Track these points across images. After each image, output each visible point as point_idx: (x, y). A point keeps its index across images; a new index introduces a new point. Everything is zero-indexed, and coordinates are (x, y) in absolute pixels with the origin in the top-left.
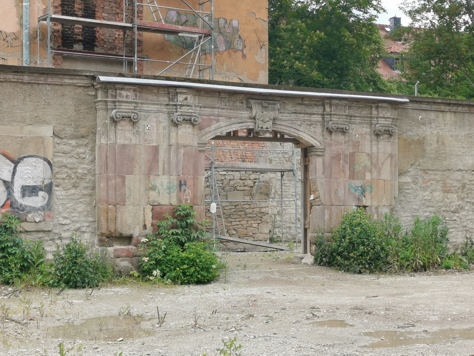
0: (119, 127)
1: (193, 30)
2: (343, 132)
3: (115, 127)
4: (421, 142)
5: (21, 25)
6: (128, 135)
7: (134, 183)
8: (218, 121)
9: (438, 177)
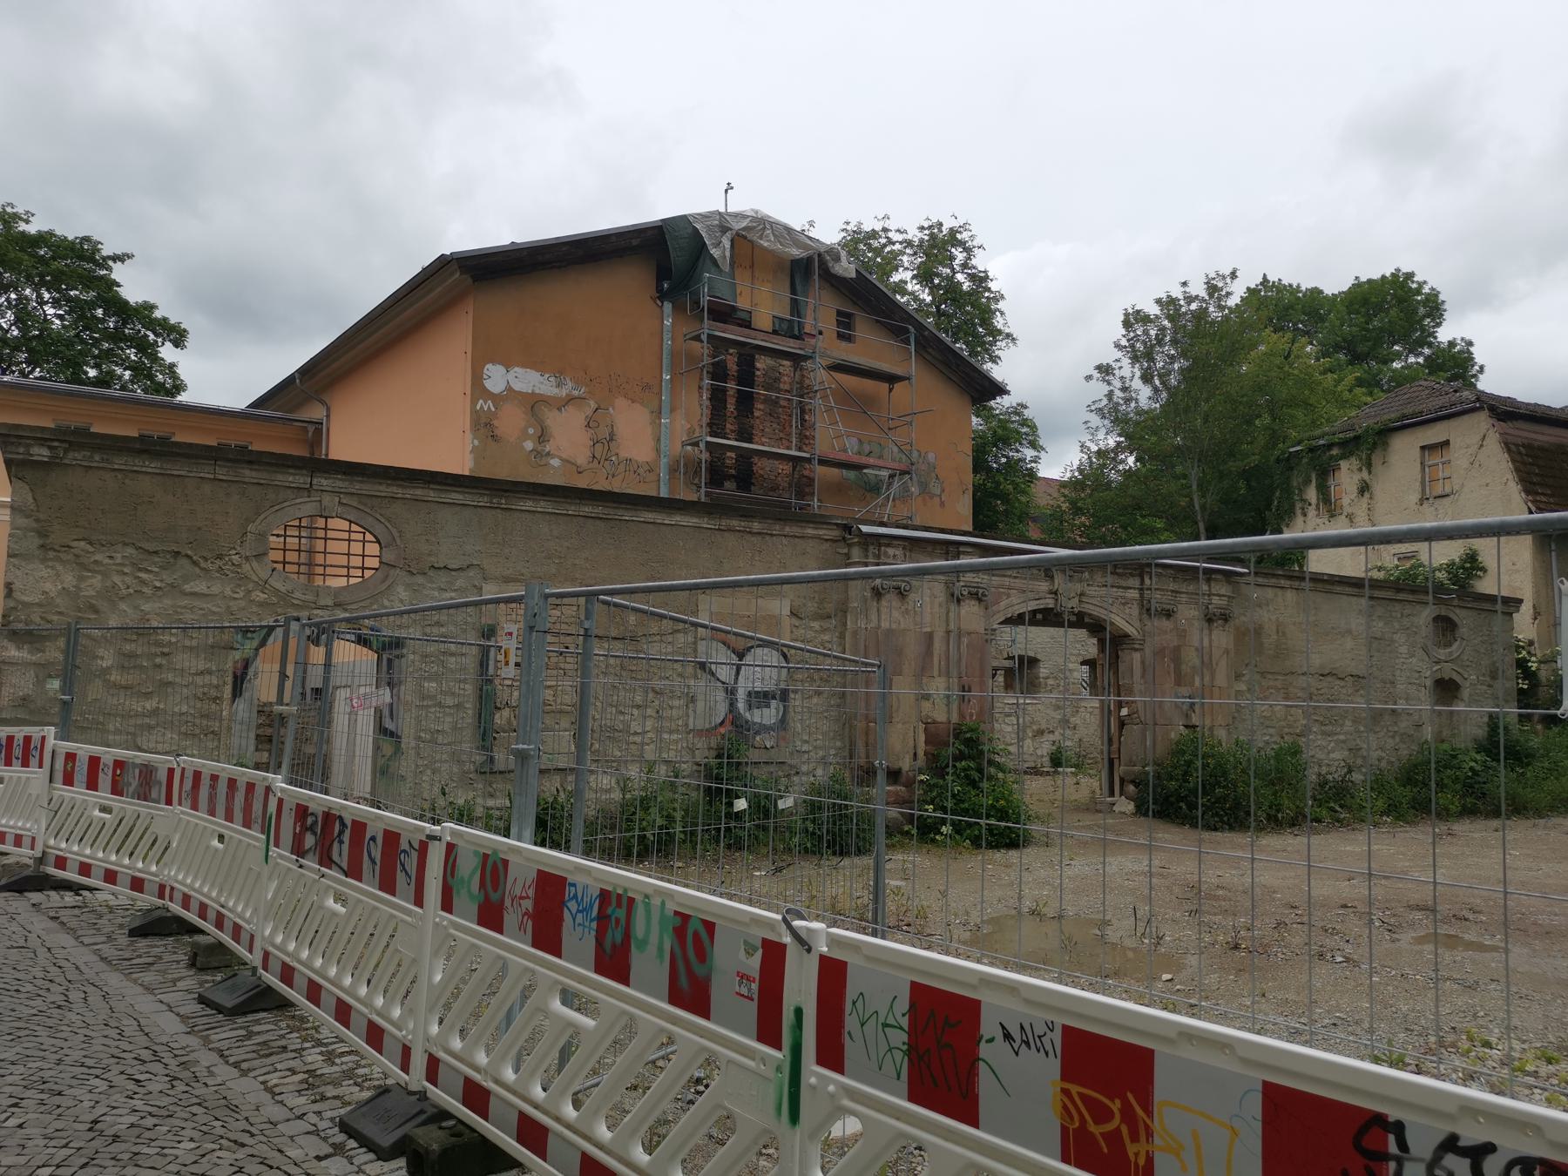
0: (884, 603)
1: (880, 463)
2: (1169, 614)
3: (878, 601)
4: (1259, 631)
5: (658, 451)
6: (896, 614)
7: (903, 689)
8: (1009, 596)
9: (1278, 684)
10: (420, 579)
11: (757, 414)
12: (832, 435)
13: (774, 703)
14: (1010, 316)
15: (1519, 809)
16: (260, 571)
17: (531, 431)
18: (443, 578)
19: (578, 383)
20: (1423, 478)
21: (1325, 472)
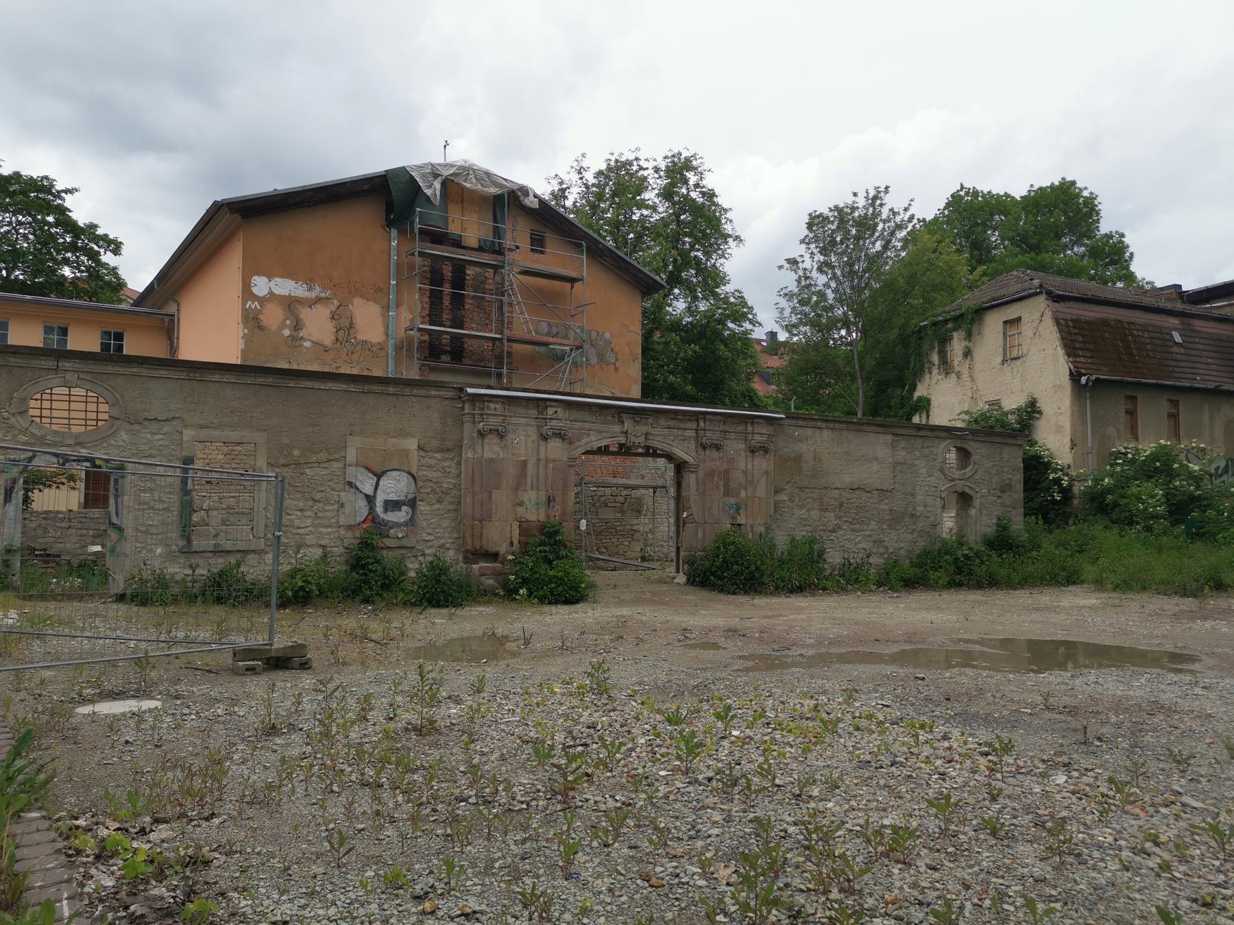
1: (564, 342)
2: (718, 447)
4: (798, 459)
7: (502, 498)
8: (589, 435)
10: (137, 427)
11: (467, 307)
12: (525, 322)
13: (404, 508)
14: (734, 222)
15: (1010, 584)
16: (23, 422)
17: (288, 322)
18: (154, 426)
19: (324, 289)
20: (1005, 345)
21: (944, 341)
